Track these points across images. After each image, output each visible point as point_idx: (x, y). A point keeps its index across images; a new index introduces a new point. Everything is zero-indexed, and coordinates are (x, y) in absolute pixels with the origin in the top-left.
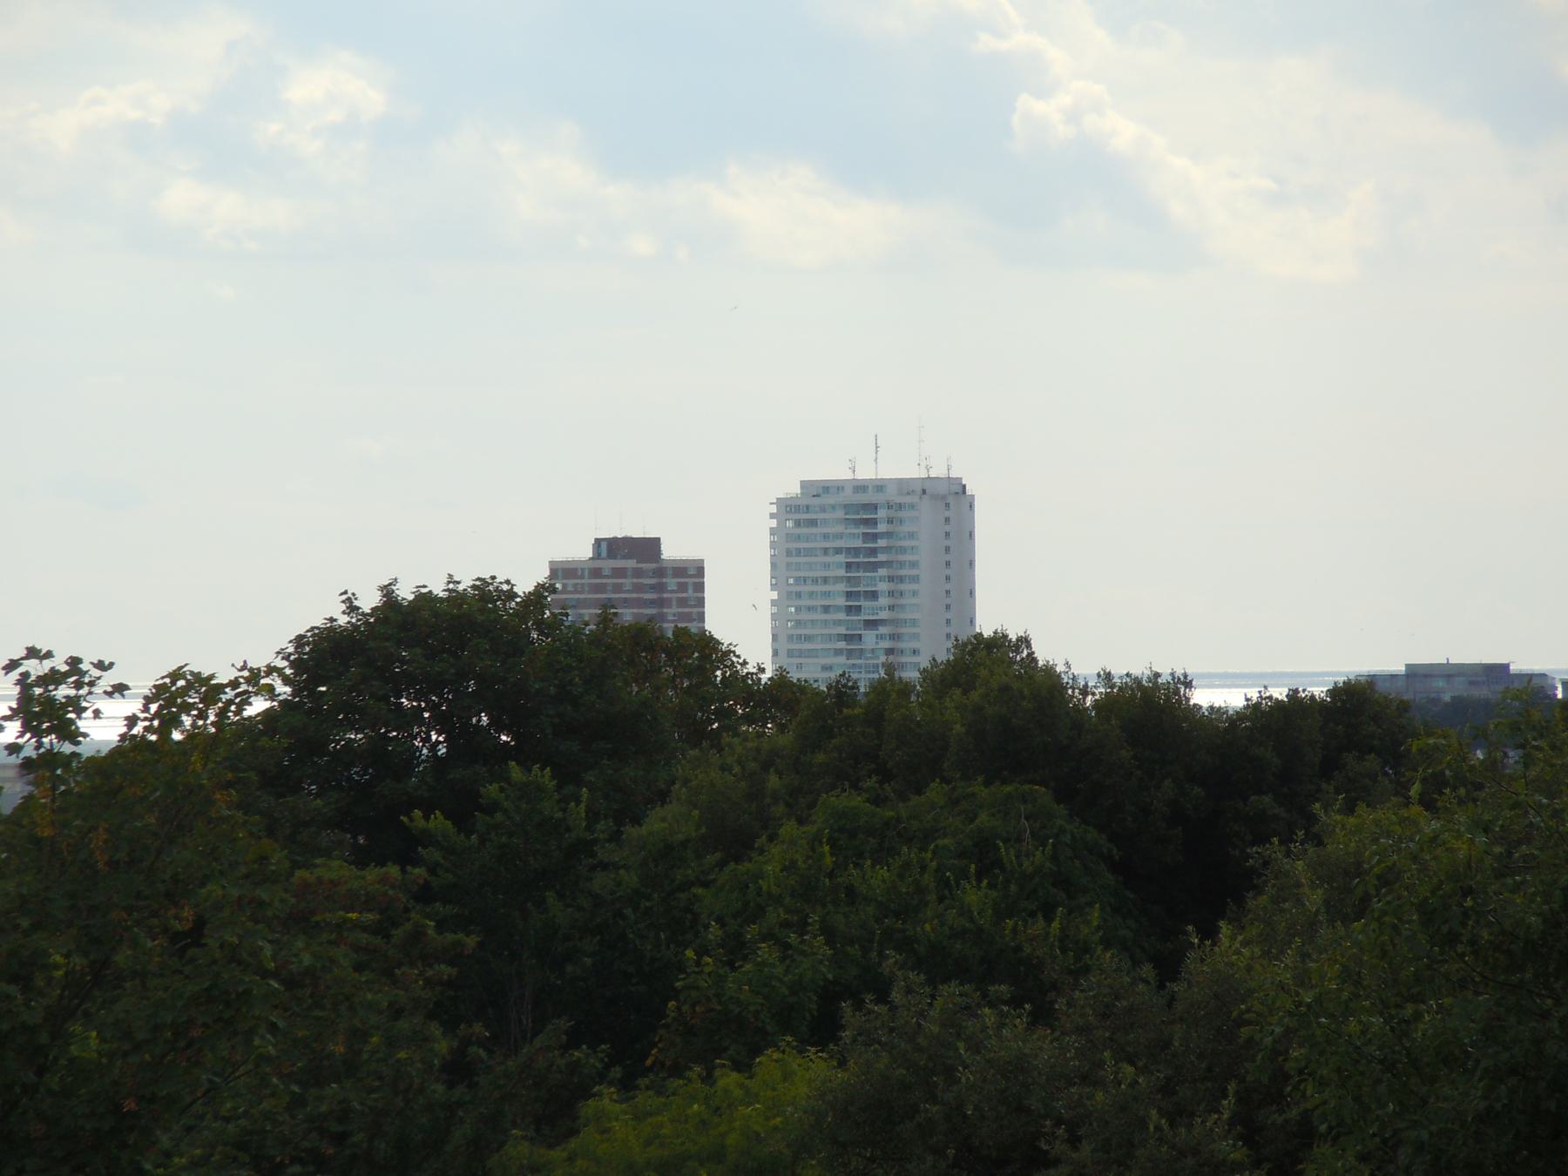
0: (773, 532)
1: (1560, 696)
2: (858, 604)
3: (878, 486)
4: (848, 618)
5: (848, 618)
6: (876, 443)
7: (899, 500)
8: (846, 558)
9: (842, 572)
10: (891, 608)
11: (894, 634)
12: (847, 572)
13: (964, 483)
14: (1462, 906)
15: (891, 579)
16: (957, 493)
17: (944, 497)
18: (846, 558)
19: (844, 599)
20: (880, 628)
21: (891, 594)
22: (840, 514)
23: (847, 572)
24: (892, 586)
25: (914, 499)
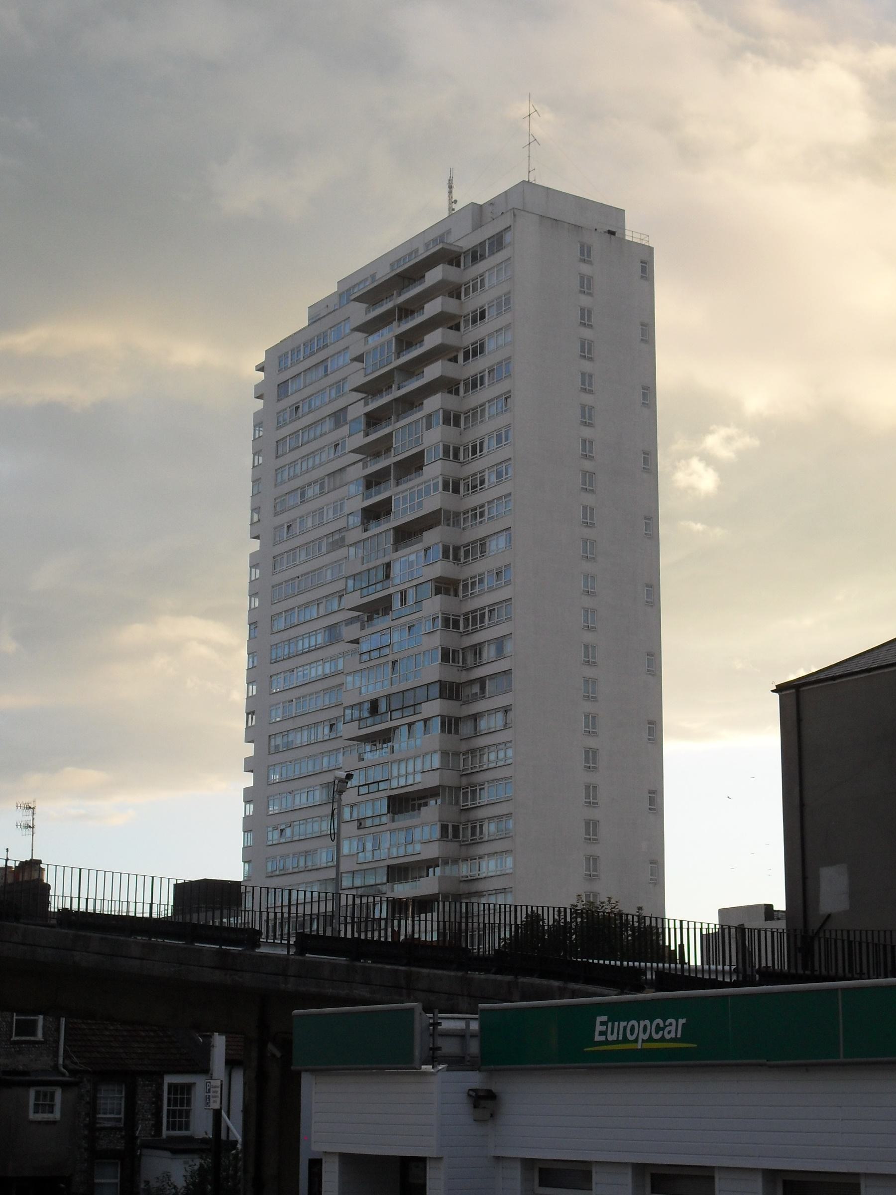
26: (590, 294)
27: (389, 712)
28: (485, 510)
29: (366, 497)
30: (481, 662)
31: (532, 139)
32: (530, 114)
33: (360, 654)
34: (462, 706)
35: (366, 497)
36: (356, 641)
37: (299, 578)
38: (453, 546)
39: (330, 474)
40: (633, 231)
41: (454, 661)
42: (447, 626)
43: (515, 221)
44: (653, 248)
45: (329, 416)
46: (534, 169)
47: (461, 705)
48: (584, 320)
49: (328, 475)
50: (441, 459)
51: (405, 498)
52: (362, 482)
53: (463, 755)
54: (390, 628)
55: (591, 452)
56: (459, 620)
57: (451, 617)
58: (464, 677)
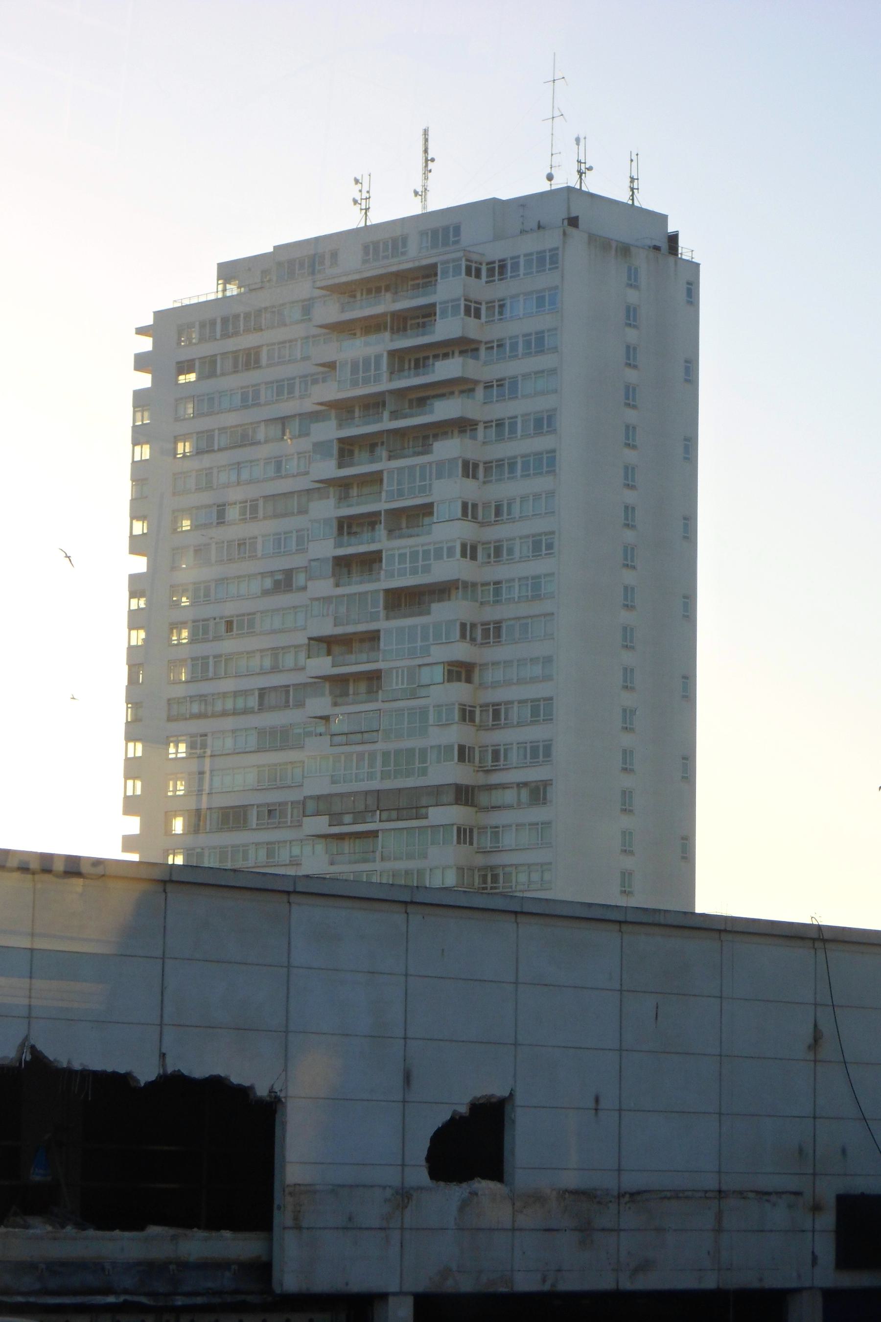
0: (141, 399)
1: (183, 679)
2: (373, 547)
3: (435, 232)
4: (340, 591)
5: (340, 591)
6: (426, 151)
7: (495, 252)
8: (340, 426)
9: (328, 468)
10: (470, 551)
11: (473, 626)
12: (340, 466)
13: (671, 229)
14: (476, 726)
15: (469, 469)
16: (657, 248)
17: (625, 250)
18: (340, 426)
19: (333, 463)
20: (435, 607)
21: (469, 510)
22: (320, 824)
23: (340, 466)
24: (470, 489)
25: (550, 240)
26: (635, 327)
27: (378, 812)
28: (282, 460)
29: (339, 545)
30: (506, 765)
31: (557, 113)
32: (554, 80)
33: (332, 735)
34: (478, 813)
35: (339, 545)
36: (326, 718)
37: (215, 619)
38: (471, 624)
39: (267, 496)
40: (686, 248)
41: (469, 761)
42: (464, 720)
43: (564, 243)
44: (698, 265)
45: (265, 421)
46: (560, 153)
47: (476, 812)
48: (629, 360)
49: (264, 497)
50: (460, 519)
51: (402, 556)
52: (335, 524)
53: (478, 871)
54: (380, 710)
55: (633, 520)
56: (474, 711)
57: (468, 708)
58: (481, 779)
